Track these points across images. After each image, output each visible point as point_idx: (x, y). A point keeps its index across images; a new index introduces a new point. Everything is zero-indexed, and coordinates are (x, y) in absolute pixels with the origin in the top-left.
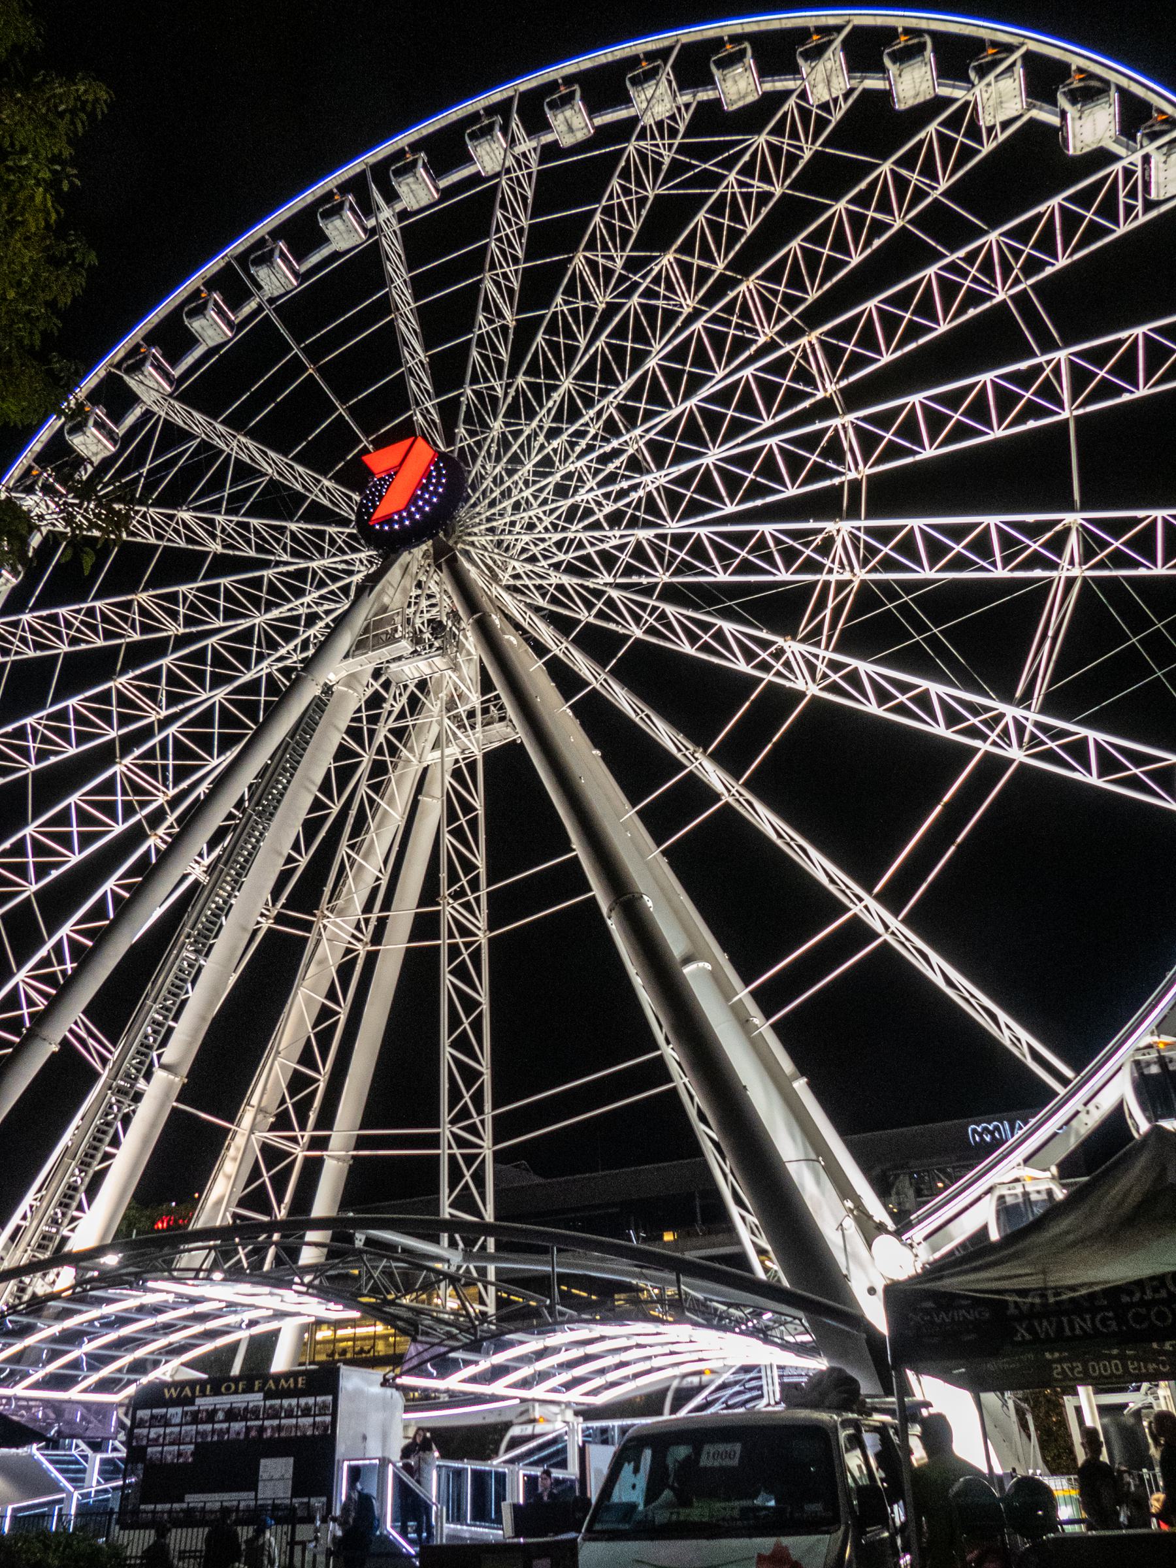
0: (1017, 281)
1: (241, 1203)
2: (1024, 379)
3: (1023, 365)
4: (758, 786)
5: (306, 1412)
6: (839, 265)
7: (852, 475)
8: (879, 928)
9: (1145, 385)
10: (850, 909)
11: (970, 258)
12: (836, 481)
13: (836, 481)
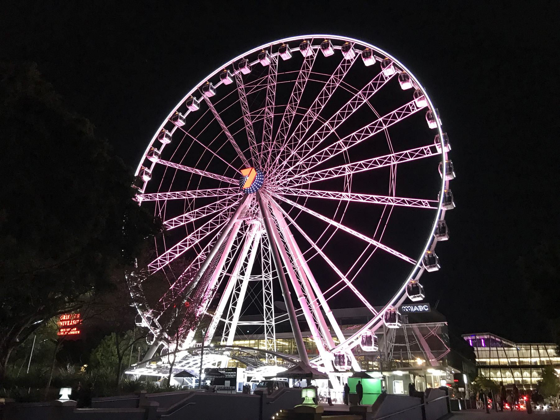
0: (339, 81)
2: (355, 99)
3: (354, 97)
5: (232, 374)
7: (344, 150)
11: (330, 82)
12: (341, 152)
13: (341, 152)
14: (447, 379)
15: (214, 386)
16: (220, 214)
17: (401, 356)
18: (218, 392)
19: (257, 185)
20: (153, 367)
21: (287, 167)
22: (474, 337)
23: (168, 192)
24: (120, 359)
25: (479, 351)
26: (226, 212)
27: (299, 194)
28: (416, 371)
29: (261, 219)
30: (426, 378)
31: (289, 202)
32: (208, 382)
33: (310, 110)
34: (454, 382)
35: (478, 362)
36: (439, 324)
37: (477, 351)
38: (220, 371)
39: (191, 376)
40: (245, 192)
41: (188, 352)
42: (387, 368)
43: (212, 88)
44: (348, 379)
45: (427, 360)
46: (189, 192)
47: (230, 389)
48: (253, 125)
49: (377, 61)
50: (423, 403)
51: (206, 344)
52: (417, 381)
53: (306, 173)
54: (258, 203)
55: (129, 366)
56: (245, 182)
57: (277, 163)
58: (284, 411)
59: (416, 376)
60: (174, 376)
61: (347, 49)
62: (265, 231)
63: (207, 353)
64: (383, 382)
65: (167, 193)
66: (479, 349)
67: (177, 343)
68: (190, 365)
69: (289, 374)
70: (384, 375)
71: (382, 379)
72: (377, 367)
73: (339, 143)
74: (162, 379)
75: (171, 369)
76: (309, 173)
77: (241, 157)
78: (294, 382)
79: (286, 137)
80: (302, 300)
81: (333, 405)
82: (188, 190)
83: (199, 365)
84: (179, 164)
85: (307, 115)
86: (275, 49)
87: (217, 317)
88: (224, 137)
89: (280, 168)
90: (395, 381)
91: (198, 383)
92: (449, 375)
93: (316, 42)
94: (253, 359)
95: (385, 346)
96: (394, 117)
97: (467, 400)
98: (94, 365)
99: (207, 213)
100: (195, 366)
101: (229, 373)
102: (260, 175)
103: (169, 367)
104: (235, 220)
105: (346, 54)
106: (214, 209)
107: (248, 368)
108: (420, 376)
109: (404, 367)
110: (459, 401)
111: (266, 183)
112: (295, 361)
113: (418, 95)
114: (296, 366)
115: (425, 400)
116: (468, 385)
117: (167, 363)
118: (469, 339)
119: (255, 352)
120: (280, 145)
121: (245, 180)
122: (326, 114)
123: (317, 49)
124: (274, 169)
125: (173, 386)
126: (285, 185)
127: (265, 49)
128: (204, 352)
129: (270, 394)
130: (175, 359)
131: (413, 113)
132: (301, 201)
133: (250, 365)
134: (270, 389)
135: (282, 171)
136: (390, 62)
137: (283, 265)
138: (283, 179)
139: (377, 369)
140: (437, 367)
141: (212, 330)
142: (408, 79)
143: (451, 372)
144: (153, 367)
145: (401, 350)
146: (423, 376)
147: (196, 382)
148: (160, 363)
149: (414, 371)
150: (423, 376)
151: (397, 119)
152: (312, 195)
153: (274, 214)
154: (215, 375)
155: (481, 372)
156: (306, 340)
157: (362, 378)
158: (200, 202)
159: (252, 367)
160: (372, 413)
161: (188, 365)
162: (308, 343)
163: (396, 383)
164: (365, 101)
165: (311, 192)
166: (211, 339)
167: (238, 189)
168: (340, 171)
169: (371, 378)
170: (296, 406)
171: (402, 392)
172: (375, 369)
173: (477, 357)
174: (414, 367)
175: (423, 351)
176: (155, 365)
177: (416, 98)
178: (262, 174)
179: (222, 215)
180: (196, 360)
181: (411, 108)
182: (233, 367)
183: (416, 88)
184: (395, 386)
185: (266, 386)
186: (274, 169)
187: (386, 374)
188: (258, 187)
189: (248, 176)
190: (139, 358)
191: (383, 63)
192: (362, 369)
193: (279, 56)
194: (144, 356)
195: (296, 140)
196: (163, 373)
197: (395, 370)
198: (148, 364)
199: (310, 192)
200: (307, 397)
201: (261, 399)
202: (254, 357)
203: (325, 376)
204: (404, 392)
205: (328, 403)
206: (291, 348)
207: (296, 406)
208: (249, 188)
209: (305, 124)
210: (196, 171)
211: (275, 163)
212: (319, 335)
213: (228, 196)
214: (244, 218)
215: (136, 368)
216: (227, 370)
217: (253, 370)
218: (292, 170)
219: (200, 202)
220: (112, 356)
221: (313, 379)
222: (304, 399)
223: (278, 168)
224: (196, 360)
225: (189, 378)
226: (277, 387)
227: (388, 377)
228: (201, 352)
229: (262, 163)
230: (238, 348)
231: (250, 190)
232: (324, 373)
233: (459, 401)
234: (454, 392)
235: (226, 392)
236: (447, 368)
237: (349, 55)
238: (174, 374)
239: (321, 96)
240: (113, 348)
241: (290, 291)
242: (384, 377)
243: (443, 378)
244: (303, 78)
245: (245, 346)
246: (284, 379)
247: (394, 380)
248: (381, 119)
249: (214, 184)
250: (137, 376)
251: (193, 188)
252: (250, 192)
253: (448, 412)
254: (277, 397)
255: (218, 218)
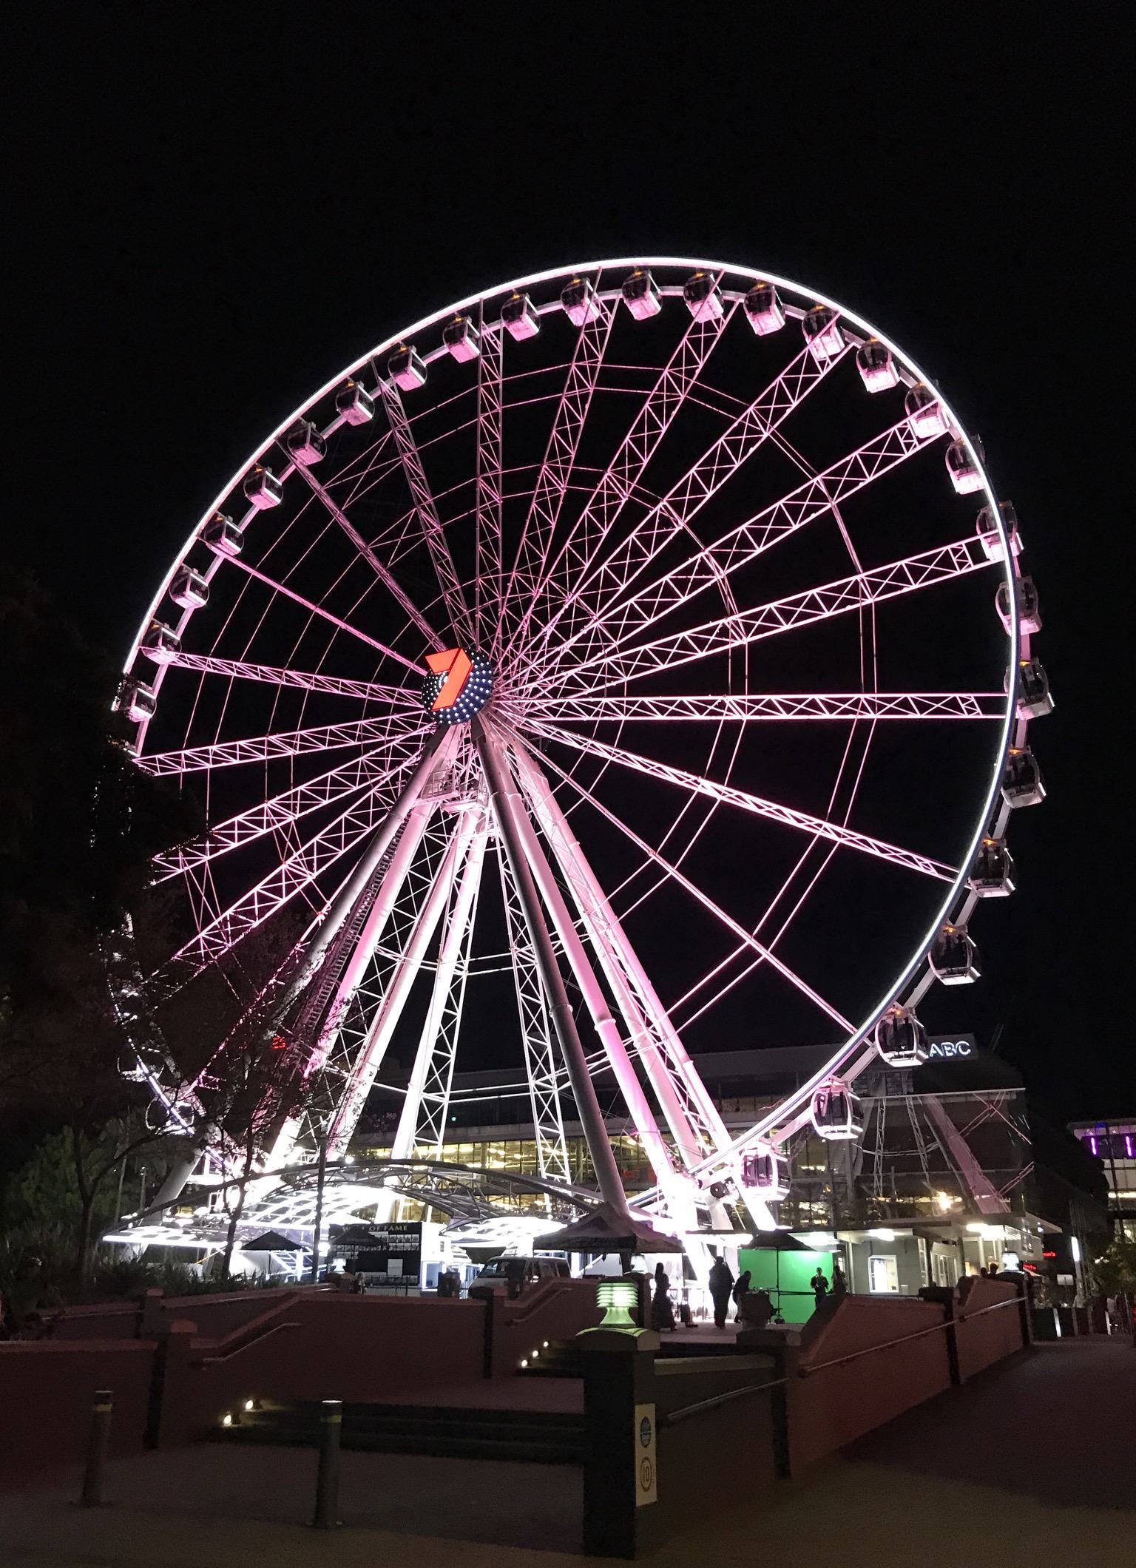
1: (426, 1091)
4: (382, 653)
5: (408, 1241)
6: (655, 437)
8: (606, 756)
9: (794, 399)
10: (694, 791)
11: (661, 389)
14: (1024, 1249)
15: (357, 1274)
16: (371, 793)
17: (893, 1186)
18: (370, 1292)
19: (472, 700)
20: (181, 1223)
21: (555, 641)
22: (1102, 1131)
23: (212, 744)
24: (87, 1200)
25: (1118, 1169)
26: (386, 785)
27: (597, 714)
28: (935, 1228)
29: (484, 793)
30: (962, 1247)
31: (570, 739)
32: (339, 1265)
33: (609, 473)
34: (1042, 1259)
35: (1116, 1201)
36: (1002, 1094)
37: (1113, 1169)
38: (372, 1233)
39: (292, 1246)
40: (439, 719)
41: (282, 1179)
42: (850, 1219)
43: (362, 399)
44: (739, 1251)
45: (968, 1197)
46: (273, 738)
47: (404, 1281)
48: (444, 532)
49: (788, 319)
50: (952, 1319)
51: (332, 1156)
52: (936, 1256)
53: (613, 652)
54: (477, 754)
55: (116, 1219)
56: (439, 691)
57: (525, 633)
58: (556, 1345)
59: (935, 1244)
60: (244, 1248)
61: (699, 291)
62: (497, 833)
63: (336, 1183)
64: (840, 1259)
65: (210, 748)
66: (1118, 1163)
67: (250, 1153)
68: (289, 1215)
69: (569, 1240)
70: (841, 1241)
71: (836, 1251)
72: (823, 1217)
73: (702, 558)
74: (209, 1255)
75: (232, 1228)
76: (621, 652)
77: (419, 624)
78: (584, 1263)
79: (544, 558)
80: (605, 1028)
81: (696, 1326)
82: (272, 733)
83: (313, 1215)
84: (238, 661)
85: (602, 488)
86: (493, 310)
87: (363, 1081)
88: (365, 571)
89: (536, 647)
90: (873, 1257)
91: (311, 1268)
92: (1029, 1240)
93: (609, 280)
94: (468, 1198)
95: (848, 1159)
96: (781, 519)
97: (1077, 1310)
98: (649, 1275)
99: (333, 794)
100: (304, 1219)
101: (399, 1236)
102: (480, 669)
103: (228, 1222)
104: (411, 802)
105: (698, 306)
106: (352, 780)
107: (452, 1221)
108: (946, 1242)
109: (901, 1216)
110: (1055, 1311)
111: (498, 692)
112: (589, 1201)
113: (919, 403)
114: (592, 1217)
115: (957, 1310)
116: (1084, 1269)
117: (223, 1211)
118: (1090, 1135)
119: (475, 1178)
120: (528, 580)
121: (437, 685)
122: (658, 480)
123: (614, 301)
124: (517, 650)
125: (239, 1276)
126: (554, 693)
127: (463, 313)
128: (326, 1178)
129: (513, 1295)
130: (242, 1200)
131: (907, 455)
132: (605, 733)
133: (457, 1214)
134: (517, 1283)
135: (542, 655)
136: (829, 319)
137: (551, 928)
138: (546, 676)
139: (824, 1222)
140: (996, 1215)
141: (347, 1118)
142: (885, 361)
143: (1035, 1232)
144: (181, 1223)
145: (893, 1168)
146: (954, 1243)
147: (306, 1263)
148: (202, 1211)
149: (928, 1228)
150: (954, 1243)
151: (865, 477)
152: (635, 714)
153: (522, 783)
154: (361, 1244)
155: (1123, 1230)
156: (621, 1141)
157: (778, 1250)
158: (310, 766)
159: (464, 1222)
160: (804, 1348)
161: (282, 1217)
162: (624, 1149)
163: (876, 1262)
164: (765, 435)
165: (632, 703)
166: (346, 1140)
167: (417, 717)
168: (712, 638)
169: (806, 1250)
170: (582, 1332)
171: (894, 1288)
172: (816, 1222)
173: (1112, 1186)
174: (928, 1218)
175: (955, 1171)
176: (190, 1215)
177: (912, 412)
178: (487, 668)
179: (378, 794)
180: (305, 1202)
181: (902, 441)
182: (409, 1221)
183: (910, 384)
184: (873, 1271)
185: (504, 1274)
186: (517, 650)
187: (846, 1236)
188: (477, 704)
189: (447, 674)
190: (143, 1196)
191: (808, 322)
192: (779, 1223)
193: (505, 329)
194: (156, 1191)
195: (575, 563)
196: (212, 1239)
197: (875, 1227)
198: (169, 1213)
199: (628, 703)
200: (611, 1305)
201: (489, 1311)
202: (471, 1190)
203: (672, 1245)
204: (900, 1289)
205: (682, 1321)
206: (578, 1166)
207: (582, 1332)
208: (451, 707)
209: (598, 513)
210: (290, 679)
211: (520, 634)
212: (655, 1128)
213: (389, 741)
214: (438, 794)
215: (135, 1226)
216: (392, 1227)
217: (469, 1228)
218: (571, 648)
219: (310, 766)
220: (67, 1191)
221: (638, 1254)
222: (603, 1311)
223: (529, 646)
224: (305, 1202)
225: (286, 1252)
226: (535, 1277)
227: (853, 1244)
228: (316, 1178)
229: (482, 636)
230: (426, 1167)
231: (452, 713)
232: (669, 1235)
233: (1055, 1311)
234: (1045, 1285)
235: (390, 1292)
236: (1023, 1220)
237: (709, 310)
238: (243, 1241)
239: (639, 429)
240: (68, 1170)
241: (571, 1003)
242: (842, 1247)
243: (1009, 1247)
244: (582, 385)
245: (446, 1161)
246: (556, 1255)
247: (872, 1254)
248: (818, 480)
249: (347, 709)
250: (136, 1250)
251: (285, 724)
252: (454, 719)
253: (1024, 1343)
254: (531, 1308)
255: (365, 805)
